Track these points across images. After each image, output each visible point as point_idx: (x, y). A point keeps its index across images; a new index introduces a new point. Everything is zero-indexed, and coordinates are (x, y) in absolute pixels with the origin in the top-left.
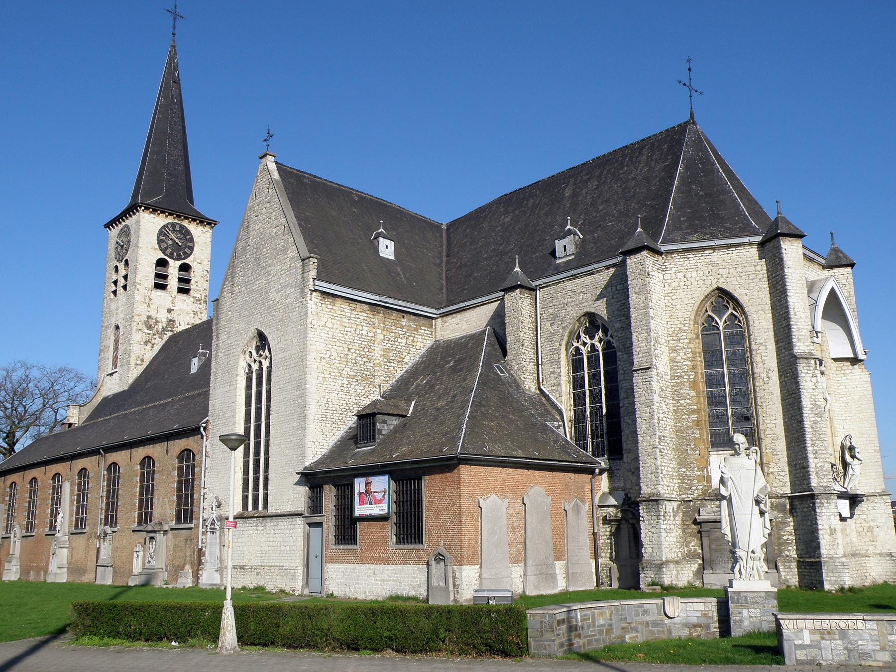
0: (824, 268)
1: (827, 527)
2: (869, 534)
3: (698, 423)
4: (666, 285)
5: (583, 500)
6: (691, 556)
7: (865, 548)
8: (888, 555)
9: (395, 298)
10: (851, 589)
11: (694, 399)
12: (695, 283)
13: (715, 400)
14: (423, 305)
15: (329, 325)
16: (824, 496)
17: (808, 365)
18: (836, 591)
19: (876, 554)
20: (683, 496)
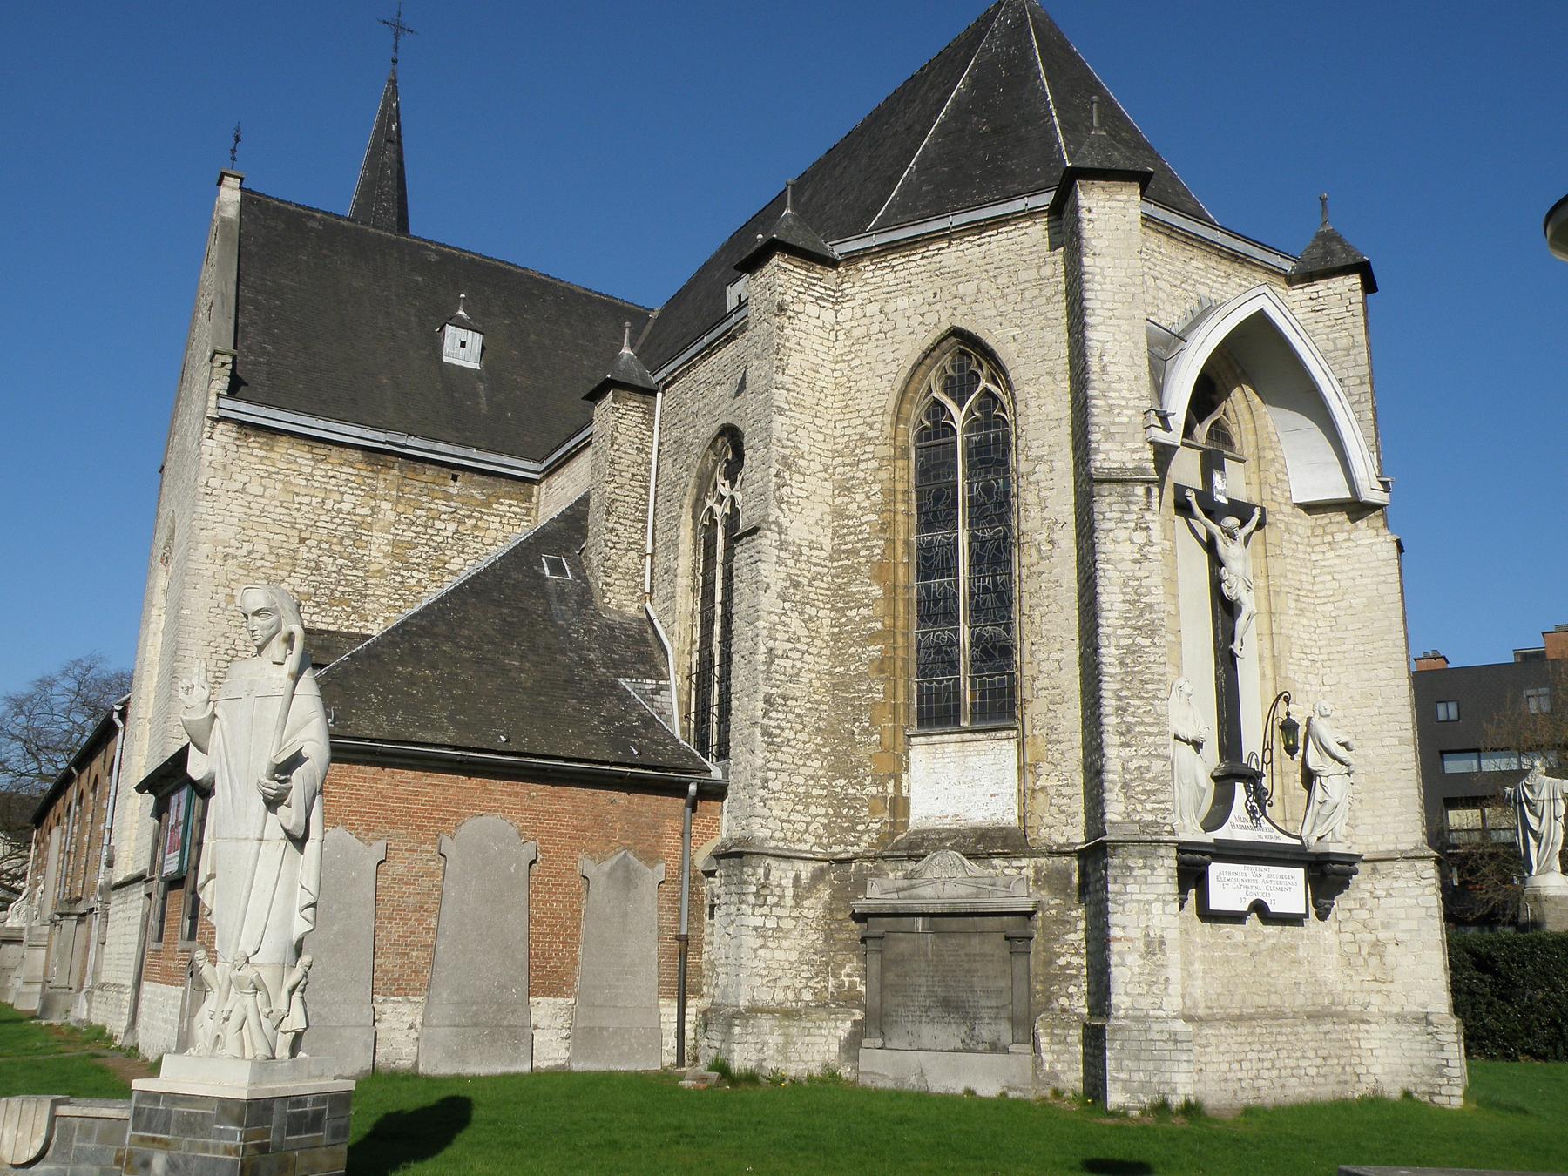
0: (1290, 281)
1: (1137, 933)
2: (1374, 961)
3: (882, 666)
4: (841, 337)
5: (651, 858)
6: (847, 999)
7: (1361, 998)
8: (1418, 1020)
9: (423, 437)
10: (1192, 1109)
11: (880, 606)
12: (902, 323)
13: (936, 609)
14: (500, 453)
15: (255, 488)
16: (1134, 849)
17: (1127, 499)
18: (1144, 1111)
19: (1387, 1016)
20: (836, 849)
